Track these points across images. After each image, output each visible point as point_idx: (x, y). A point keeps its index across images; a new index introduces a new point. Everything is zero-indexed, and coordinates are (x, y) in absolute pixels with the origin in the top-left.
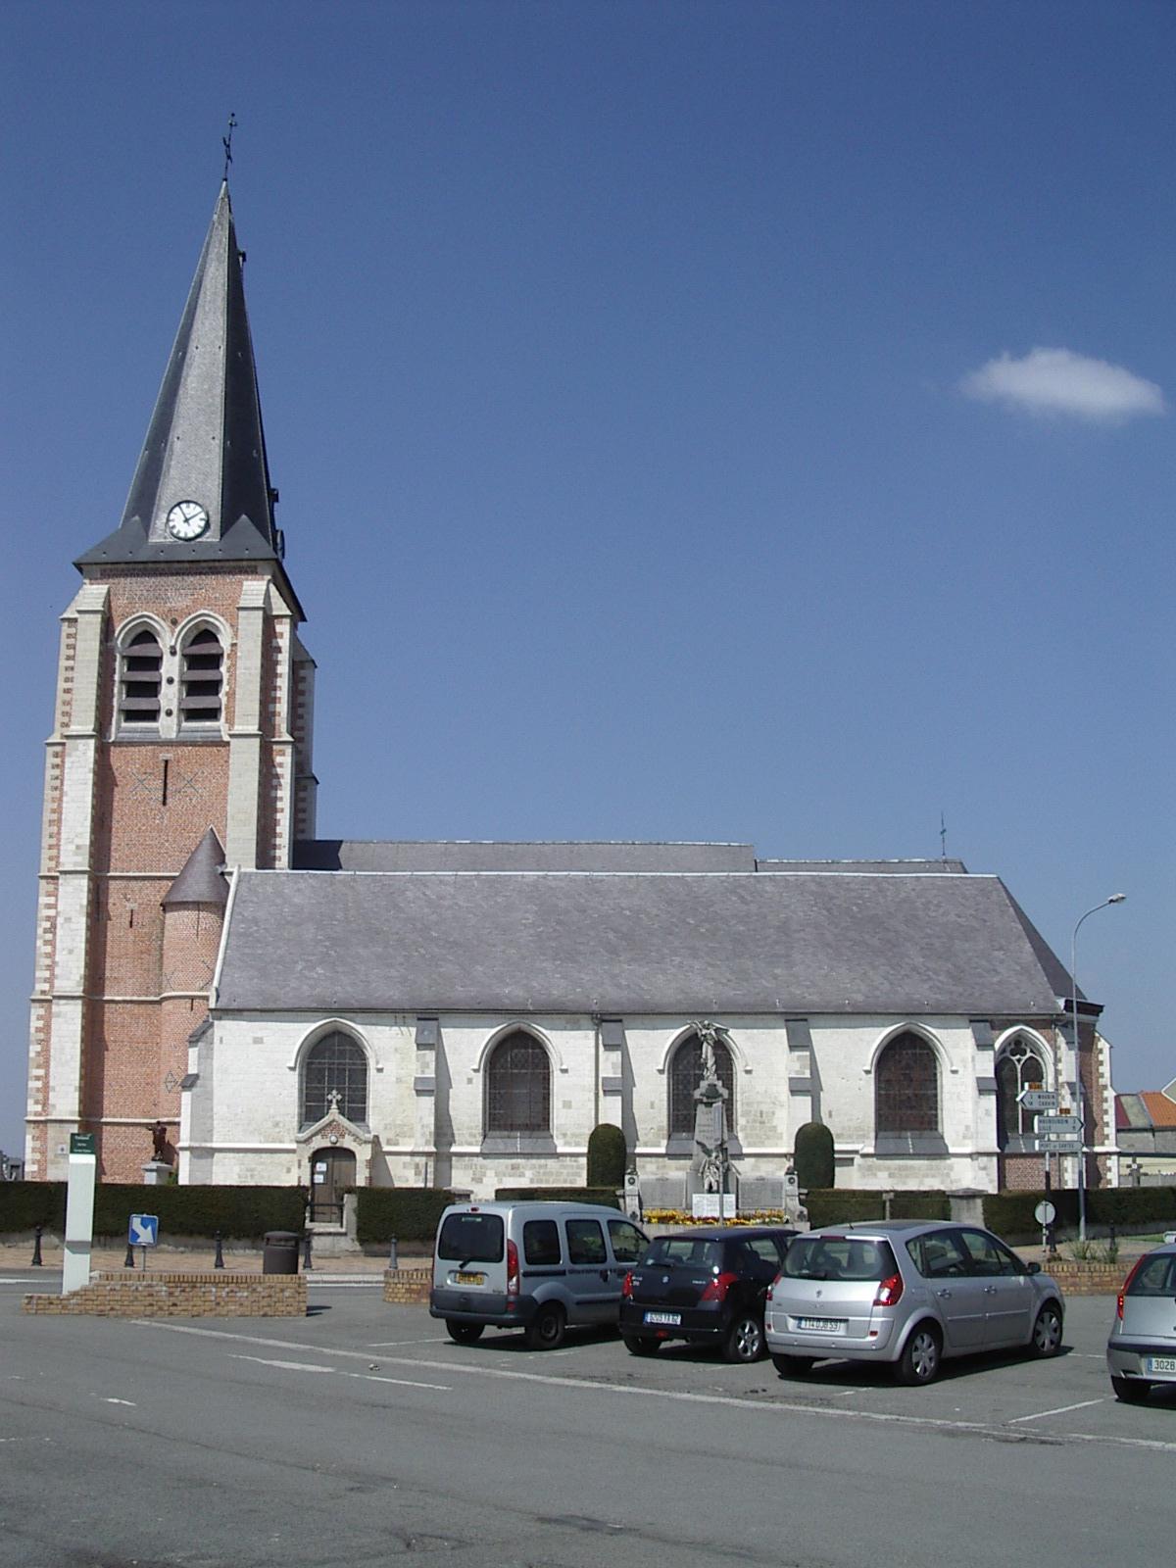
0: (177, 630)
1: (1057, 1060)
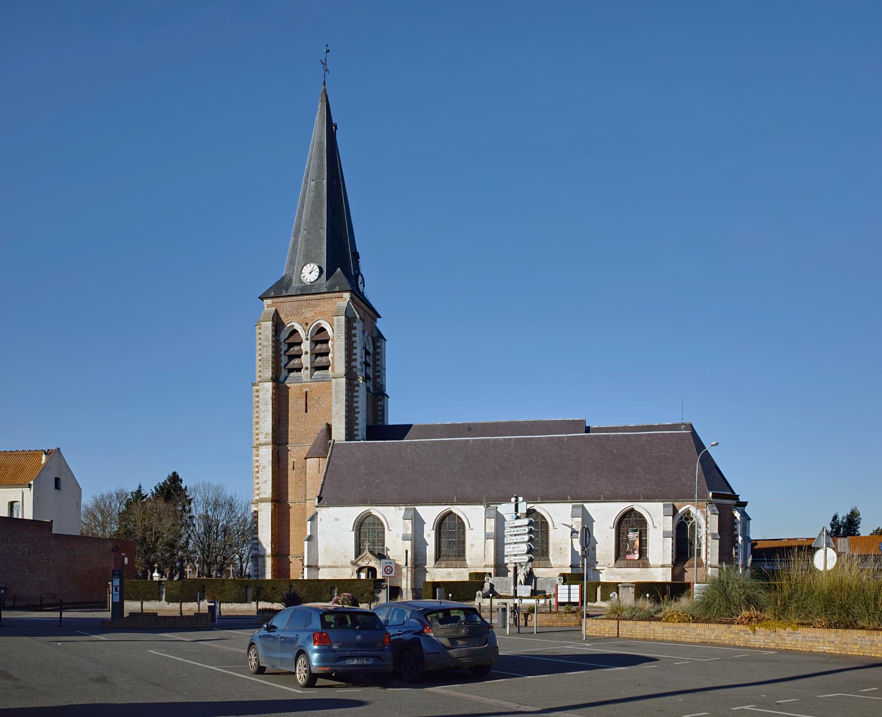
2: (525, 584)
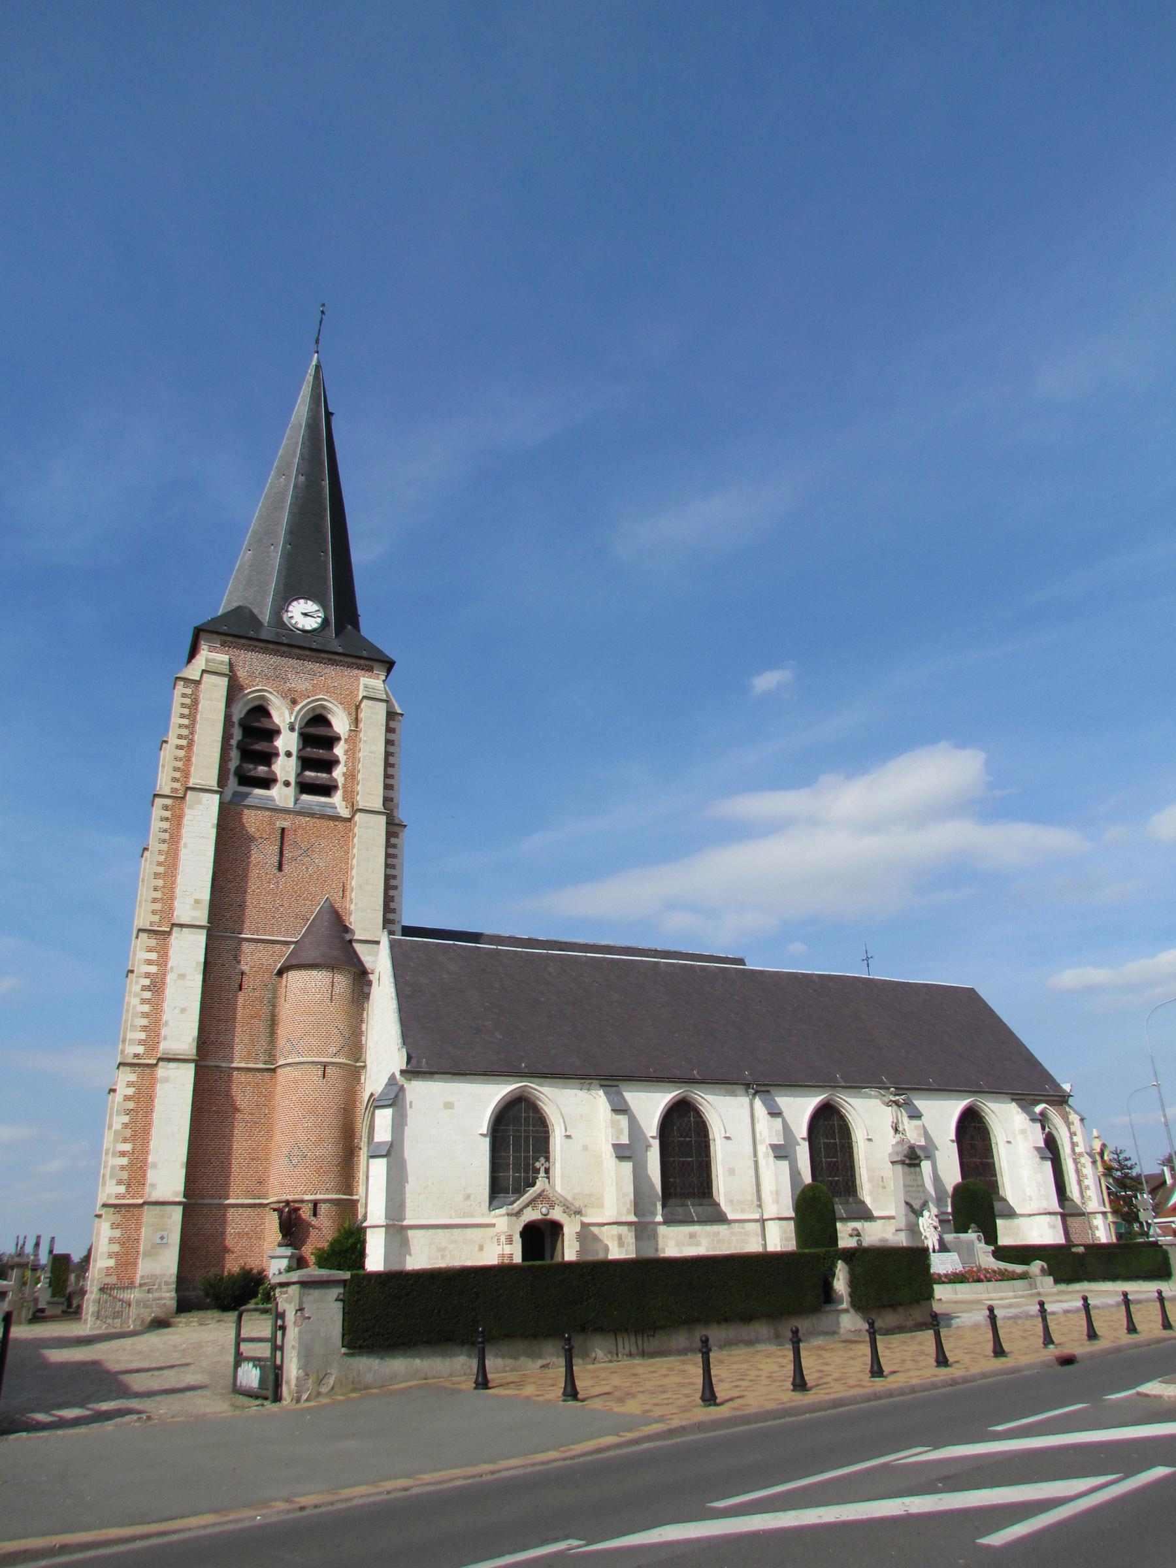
0: (297, 708)
1: (1072, 1134)
2: (939, 1252)
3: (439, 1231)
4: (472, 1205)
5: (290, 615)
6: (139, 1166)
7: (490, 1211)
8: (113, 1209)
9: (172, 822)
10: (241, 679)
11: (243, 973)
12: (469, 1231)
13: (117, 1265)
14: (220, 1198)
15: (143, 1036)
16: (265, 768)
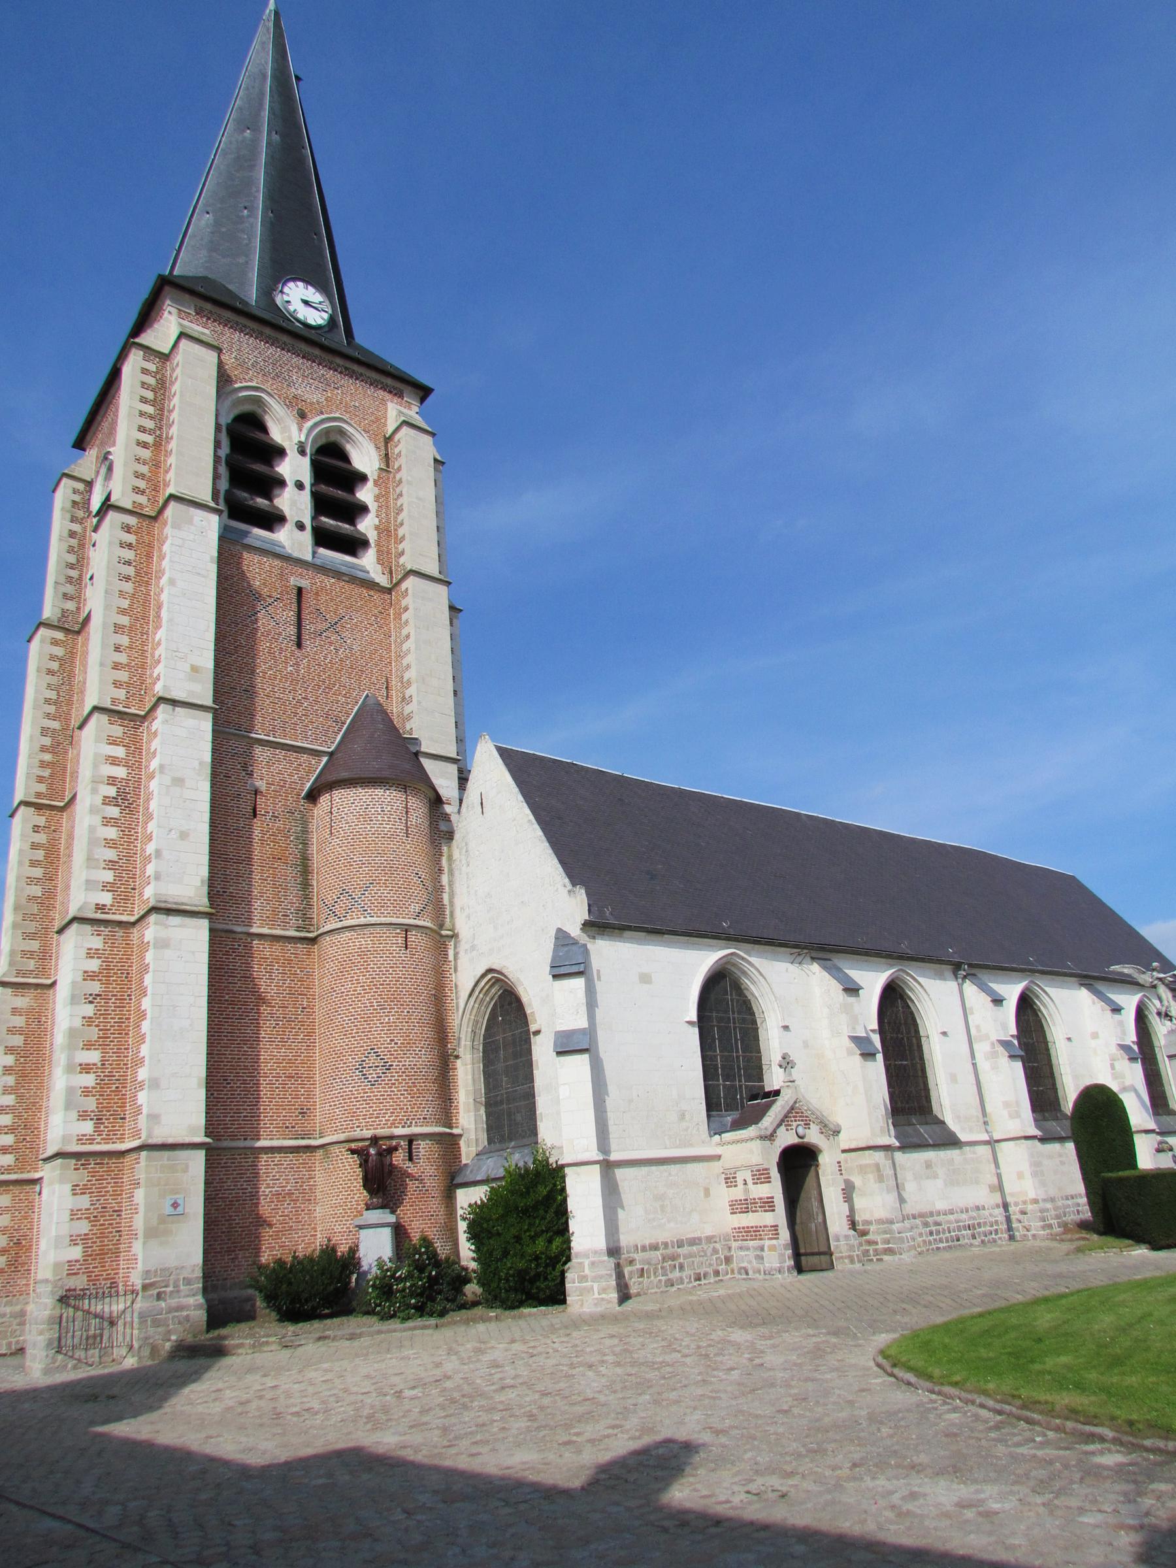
3: (654, 1168)
4: (687, 1128)
5: (286, 298)
6: (114, 1089)
7: (711, 1136)
8: (74, 1161)
9: (138, 552)
10: (227, 367)
11: (256, 792)
12: (690, 1167)
13: (86, 1255)
14: (245, 1139)
15: (109, 876)
16: (266, 502)
